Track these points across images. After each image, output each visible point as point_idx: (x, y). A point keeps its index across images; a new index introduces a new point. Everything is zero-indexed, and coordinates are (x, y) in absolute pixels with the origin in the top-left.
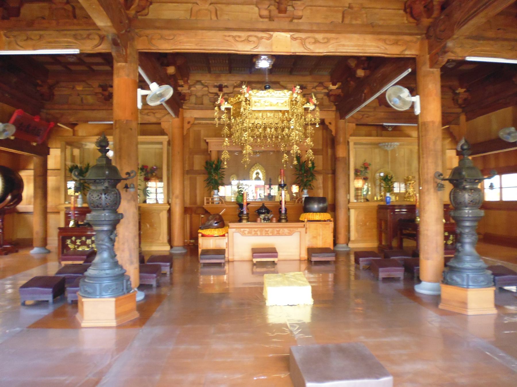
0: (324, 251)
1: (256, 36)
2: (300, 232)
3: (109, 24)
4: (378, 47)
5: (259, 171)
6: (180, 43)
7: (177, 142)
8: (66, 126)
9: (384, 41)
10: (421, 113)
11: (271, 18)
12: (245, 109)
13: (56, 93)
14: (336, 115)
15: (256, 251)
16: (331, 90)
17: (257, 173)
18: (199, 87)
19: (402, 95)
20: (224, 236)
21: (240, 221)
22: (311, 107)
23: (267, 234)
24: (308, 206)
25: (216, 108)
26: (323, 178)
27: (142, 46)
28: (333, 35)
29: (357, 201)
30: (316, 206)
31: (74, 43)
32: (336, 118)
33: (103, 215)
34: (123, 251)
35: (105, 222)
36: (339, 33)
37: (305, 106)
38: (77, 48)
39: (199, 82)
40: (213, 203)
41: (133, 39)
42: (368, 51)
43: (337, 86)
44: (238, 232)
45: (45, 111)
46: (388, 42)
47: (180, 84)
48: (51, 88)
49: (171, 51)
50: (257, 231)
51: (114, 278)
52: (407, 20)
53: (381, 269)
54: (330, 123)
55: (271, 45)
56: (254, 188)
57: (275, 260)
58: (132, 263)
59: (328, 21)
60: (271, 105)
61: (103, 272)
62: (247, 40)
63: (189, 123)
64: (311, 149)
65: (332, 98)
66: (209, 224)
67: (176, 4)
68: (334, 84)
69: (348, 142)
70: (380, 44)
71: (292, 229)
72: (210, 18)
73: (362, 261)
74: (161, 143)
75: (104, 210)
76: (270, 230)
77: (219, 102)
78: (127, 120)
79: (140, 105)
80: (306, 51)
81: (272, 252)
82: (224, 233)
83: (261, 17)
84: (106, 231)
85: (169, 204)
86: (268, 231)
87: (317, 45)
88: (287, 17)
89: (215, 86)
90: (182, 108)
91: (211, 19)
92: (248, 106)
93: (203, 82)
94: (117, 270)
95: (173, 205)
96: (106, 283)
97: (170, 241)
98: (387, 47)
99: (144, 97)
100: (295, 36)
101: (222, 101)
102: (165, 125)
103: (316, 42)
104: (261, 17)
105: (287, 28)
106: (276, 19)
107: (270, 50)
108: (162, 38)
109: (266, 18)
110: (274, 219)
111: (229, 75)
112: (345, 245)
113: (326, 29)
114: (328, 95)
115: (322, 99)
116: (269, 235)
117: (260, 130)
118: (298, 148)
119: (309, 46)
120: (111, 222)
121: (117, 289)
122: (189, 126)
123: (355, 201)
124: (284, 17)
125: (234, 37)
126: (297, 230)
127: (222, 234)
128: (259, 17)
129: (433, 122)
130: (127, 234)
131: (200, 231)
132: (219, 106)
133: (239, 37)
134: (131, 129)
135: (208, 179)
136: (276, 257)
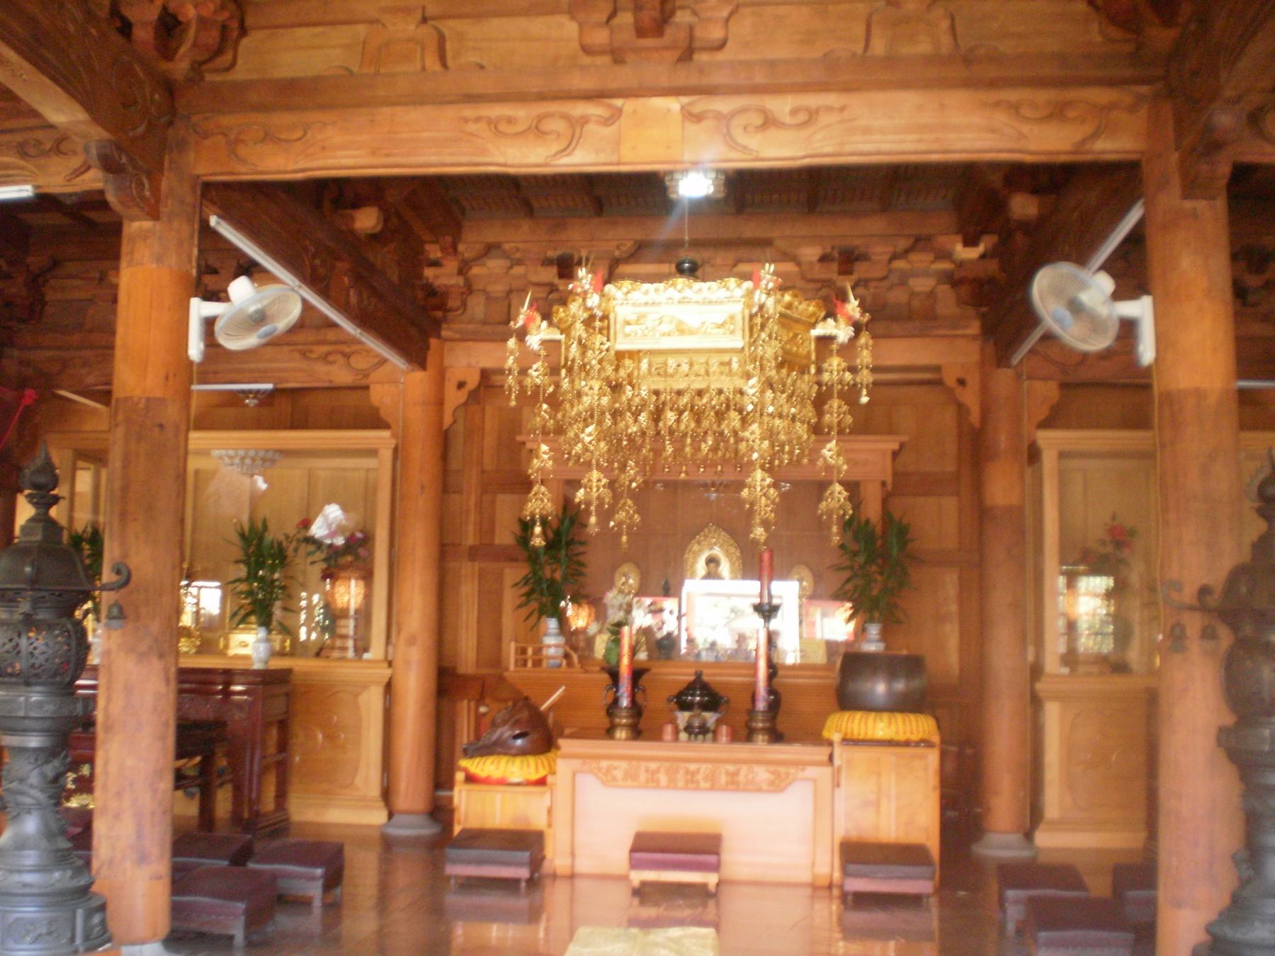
0: (904, 855)
1: (566, 117)
2: (814, 781)
3: (81, 115)
4: (993, 131)
5: (717, 551)
6: (324, 148)
7: (422, 454)
8: (85, 397)
9: (1015, 108)
10: (1157, 359)
11: (617, 55)
12: (584, 347)
13: (51, 296)
14: (982, 349)
15: (648, 846)
16: (961, 264)
17: (712, 561)
18: (495, 265)
19: (1085, 297)
20: (541, 782)
21: (609, 733)
22: (843, 333)
23: (691, 783)
24: (852, 686)
25: (512, 343)
26: (960, 578)
27: (208, 164)
28: (830, 99)
29: (1073, 670)
30: (880, 688)
31: (19, 168)
32: (982, 362)
33: (22, 699)
34: (117, 816)
35: (28, 723)
36: (847, 88)
37: (819, 331)
38: (25, 182)
39: (490, 249)
40: (538, 663)
41: (181, 145)
42: (958, 146)
43: (981, 249)
44: (591, 772)
45: (16, 353)
46: (1026, 112)
47: (432, 256)
48: (36, 282)
49: (300, 176)
50: (658, 771)
51: (46, 899)
52: (1101, 32)
53: (1043, 935)
54: (962, 382)
55: (617, 143)
56: (717, 611)
57: (711, 879)
58: (142, 859)
59: (816, 52)
60: (682, 332)
61: (16, 878)
62: (537, 131)
63: (461, 385)
64: (841, 483)
65: (964, 290)
66: (495, 737)
67: (319, 29)
68: (970, 242)
69: (1034, 455)
70: (1001, 118)
71: (782, 769)
72: (419, 66)
73: (1016, 902)
74: (373, 453)
75: (28, 684)
76: (705, 768)
77: (521, 322)
78: (148, 400)
79: (195, 350)
80: (734, 155)
81: (702, 847)
82: (542, 773)
83: (587, 50)
84: (35, 750)
85: (390, 664)
86: (698, 771)
87: (773, 133)
88: (667, 48)
89: (547, 262)
90: (439, 337)
91: (424, 68)
92: (599, 338)
93: (506, 246)
94: (57, 875)
95: (399, 662)
96: (29, 911)
97: (387, 794)
98: (1026, 129)
99: (209, 323)
100: (697, 109)
101: (530, 319)
102: (381, 395)
103: (769, 122)
104: (587, 50)
105: (664, 81)
106: (630, 58)
107: (614, 159)
108: (268, 137)
109: (603, 52)
110: (724, 729)
111: (596, 221)
112: (1015, 838)
113: (799, 78)
114: (952, 280)
115: (931, 294)
116: (697, 789)
117: (643, 417)
118: (769, 480)
119: (743, 139)
120: (47, 724)
121: (50, 933)
122: (462, 396)
123: (1065, 670)
124: (656, 49)
125: (493, 124)
126: (800, 775)
127: (534, 776)
128: (581, 53)
129: (1199, 394)
130: (129, 762)
131: (464, 763)
132: (522, 334)
133: (510, 121)
134: (161, 426)
135: (526, 581)
136: (716, 868)
